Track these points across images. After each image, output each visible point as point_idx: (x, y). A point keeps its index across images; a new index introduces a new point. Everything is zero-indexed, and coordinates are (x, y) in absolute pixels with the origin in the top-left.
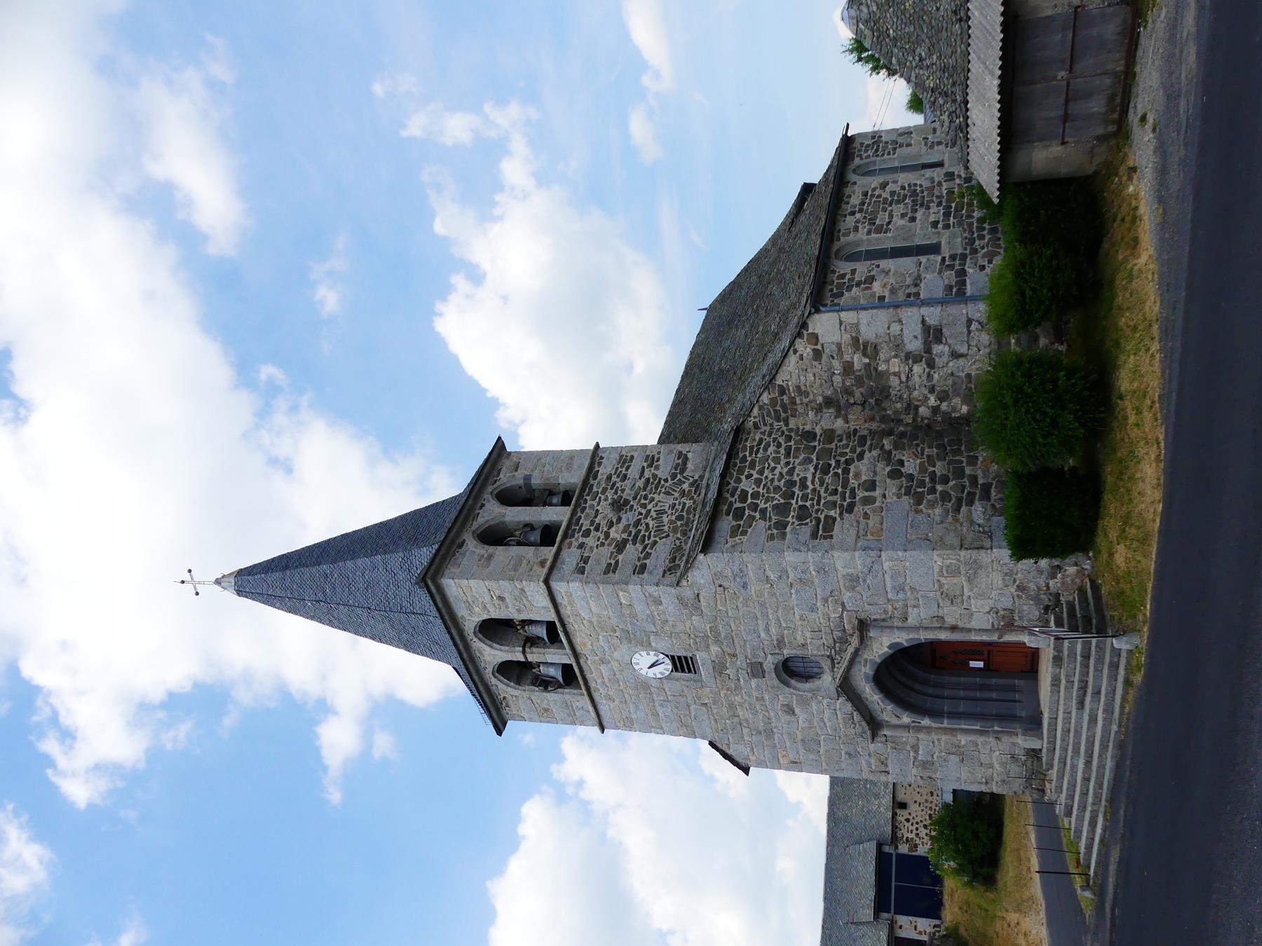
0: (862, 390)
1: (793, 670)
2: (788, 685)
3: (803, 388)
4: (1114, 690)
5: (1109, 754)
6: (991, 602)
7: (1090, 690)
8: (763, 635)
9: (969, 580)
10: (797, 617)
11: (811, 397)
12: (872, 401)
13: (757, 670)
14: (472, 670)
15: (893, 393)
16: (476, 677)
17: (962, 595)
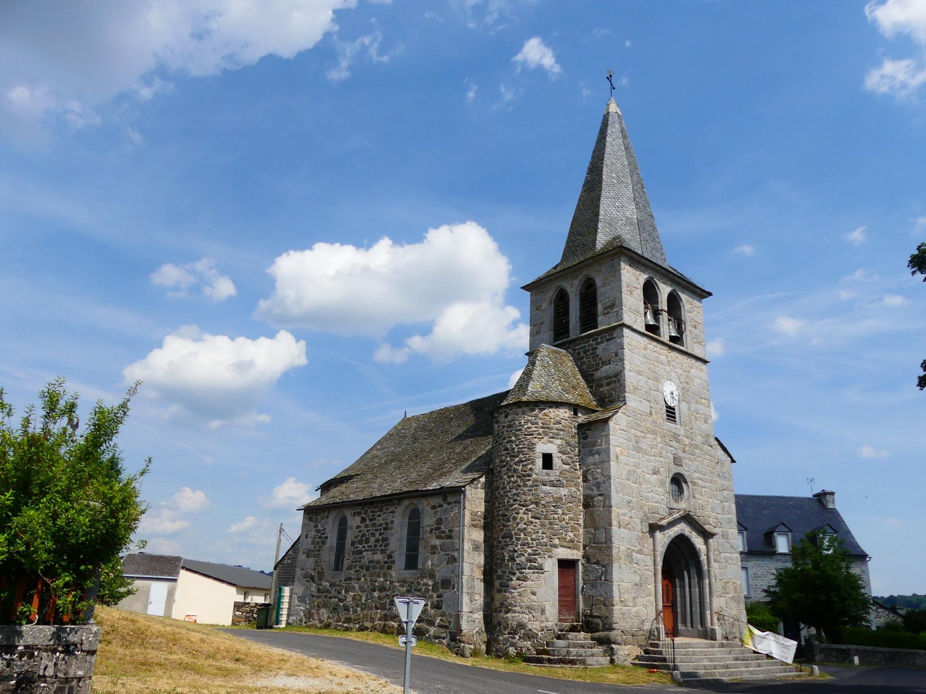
1: (678, 481)
13: (677, 461)
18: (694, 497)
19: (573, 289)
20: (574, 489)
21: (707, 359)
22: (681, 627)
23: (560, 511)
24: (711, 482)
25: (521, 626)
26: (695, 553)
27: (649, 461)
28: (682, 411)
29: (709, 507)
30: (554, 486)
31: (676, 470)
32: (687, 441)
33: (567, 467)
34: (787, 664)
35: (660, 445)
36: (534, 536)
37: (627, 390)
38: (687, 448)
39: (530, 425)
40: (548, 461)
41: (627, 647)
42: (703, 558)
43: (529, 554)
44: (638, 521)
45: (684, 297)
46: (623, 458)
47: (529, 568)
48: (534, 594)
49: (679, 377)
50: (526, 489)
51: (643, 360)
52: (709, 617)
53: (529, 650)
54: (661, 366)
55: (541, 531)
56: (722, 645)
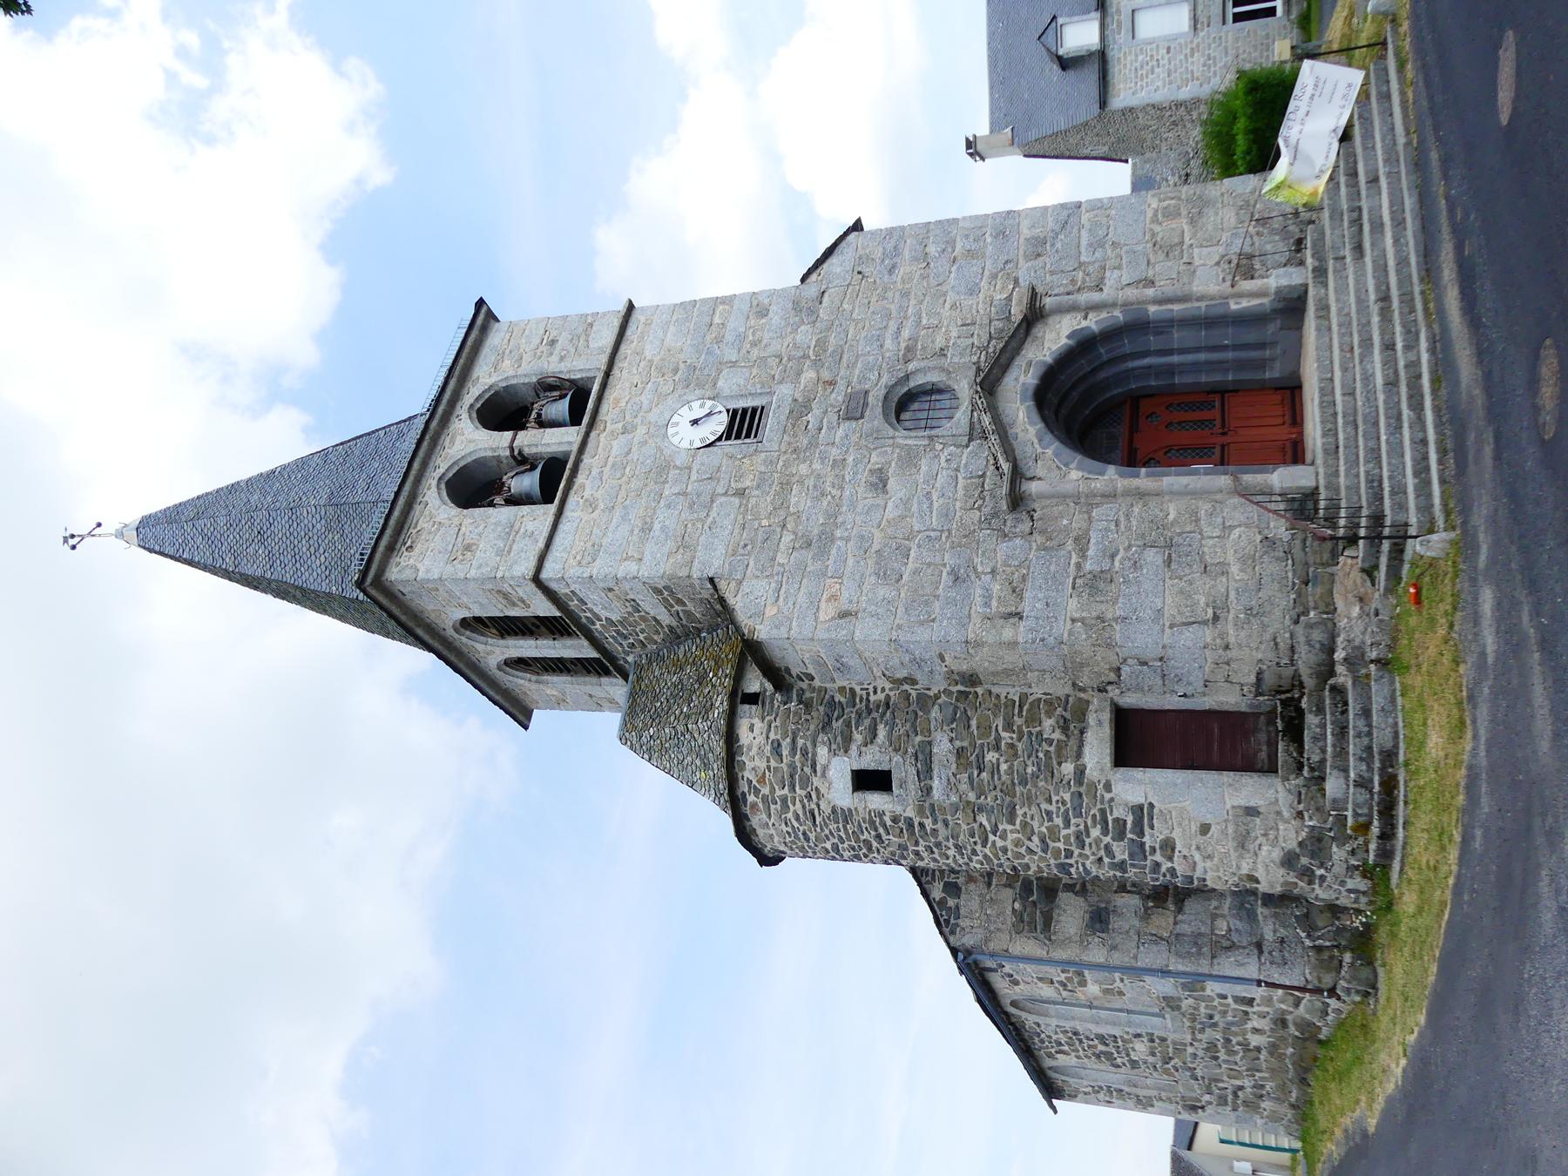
1: (908, 403)
4: (1393, 129)
5: (1409, 233)
6: (1221, 250)
7: (1362, 178)
9: (1192, 222)
10: (947, 306)
13: (854, 410)
14: (421, 454)
16: (416, 465)
17: (1182, 243)
18: (942, 353)
19: (498, 651)
20: (935, 713)
21: (622, 307)
22: (1273, 373)
23: (991, 756)
24: (905, 295)
25: (1289, 861)
26: (1084, 346)
27: (853, 506)
28: (737, 388)
29: (969, 302)
30: (930, 770)
31: (875, 417)
32: (809, 375)
33: (882, 732)
34: (1366, 83)
35: (817, 466)
36: (1059, 821)
37: (683, 573)
38: (826, 375)
39: (790, 815)
40: (867, 781)
41: (1340, 604)
42: (1093, 323)
43: (1105, 832)
44: (1004, 548)
45: (486, 377)
46: (845, 595)
47: (1141, 834)
48: (1205, 829)
49: (661, 397)
50: (943, 832)
51: (618, 513)
52: (1245, 303)
53: (1353, 852)
54: (634, 456)
55: (1044, 806)
56: (1320, 273)
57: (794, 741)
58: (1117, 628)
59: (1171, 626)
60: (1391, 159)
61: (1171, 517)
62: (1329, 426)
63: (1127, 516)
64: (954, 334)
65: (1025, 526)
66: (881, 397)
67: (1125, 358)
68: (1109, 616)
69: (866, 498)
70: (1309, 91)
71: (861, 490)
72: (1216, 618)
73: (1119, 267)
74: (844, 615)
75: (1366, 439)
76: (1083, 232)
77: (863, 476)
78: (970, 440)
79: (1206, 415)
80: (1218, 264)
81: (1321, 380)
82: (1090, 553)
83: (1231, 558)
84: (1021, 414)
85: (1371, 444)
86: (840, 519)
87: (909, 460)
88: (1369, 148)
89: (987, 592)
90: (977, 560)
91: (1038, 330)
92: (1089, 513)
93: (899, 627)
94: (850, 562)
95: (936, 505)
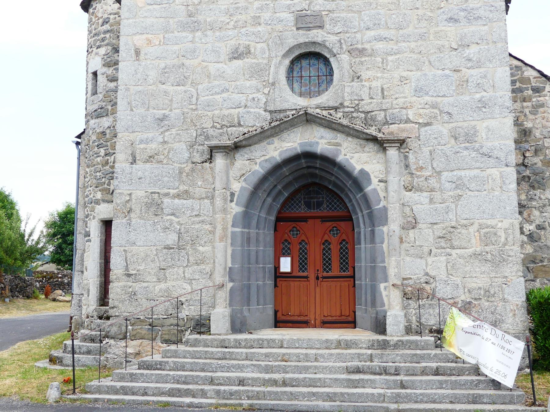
0: (540, 164)
1: (310, 62)
2: (285, 56)
3: (541, 110)
5: (320, 403)
8: (372, 33)
10: (405, 74)
11: (531, 117)
12: (527, 173)
15: (538, 192)
31: (298, 38)
57: (108, 31)
58: (124, 221)
59: (125, 251)
60: (258, 396)
61: (201, 248)
62: (243, 344)
63: (203, 222)
64: (374, 84)
65: (198, 158)
66: (315, 39)
67: (362, 212)
68: (132, 215)
69: (225, 49)
70: (507, 346)
71: (233, 42)
72: (129, 275)
73: (431, 201)
74: (137, 53)
75: (192, 363)
76: (476, 172)
77: (244, 41)
78: (271, 112)
79: (335, 264)
80: (427, 274)
81: (282, 341)
82: (176, 201)
83: (170, 284)
84: (289, 145)
85: (188, 366)
86: (209, 33)
87: (258, 72)
88: (429, 385)
89: (151, 140)
90: (174, 131)
91: (371, 147)
92: (207, 197)
93: (128, 90)
94: (176, 47)
95: (216, 97)
